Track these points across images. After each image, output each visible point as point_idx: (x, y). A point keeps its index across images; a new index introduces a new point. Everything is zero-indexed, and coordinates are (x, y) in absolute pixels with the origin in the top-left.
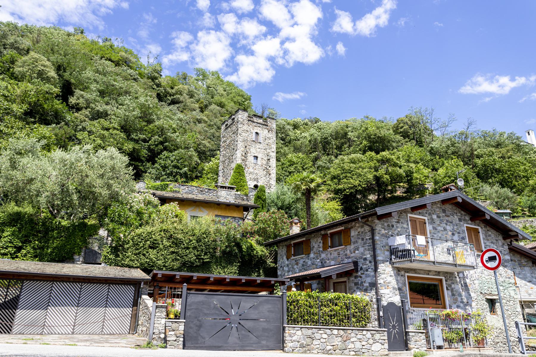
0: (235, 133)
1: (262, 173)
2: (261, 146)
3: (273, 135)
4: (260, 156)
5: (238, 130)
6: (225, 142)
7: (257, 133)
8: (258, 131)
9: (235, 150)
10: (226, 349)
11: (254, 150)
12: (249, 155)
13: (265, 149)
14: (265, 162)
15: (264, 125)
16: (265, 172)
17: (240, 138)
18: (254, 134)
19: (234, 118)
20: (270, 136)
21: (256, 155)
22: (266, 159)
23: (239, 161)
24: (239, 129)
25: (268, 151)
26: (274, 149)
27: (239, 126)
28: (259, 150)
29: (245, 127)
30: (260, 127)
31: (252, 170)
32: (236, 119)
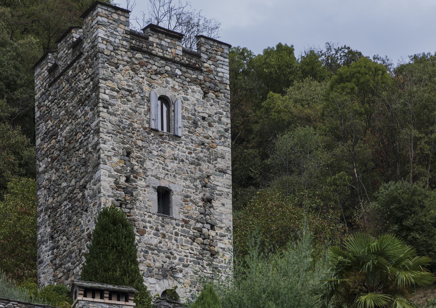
0: (90, 99)
1: (185, 250)
2: (181, 150)
3: (219, 110)
4: (178, 187)
5: (96, 88)
6: (51, 135)
7: (164, 99)
8: (169, 94)
9: (90, 164)
10: (161, 203)
11: (161, 167)
12: (141, 183)
13: (197, 163)
14: (194, 211)
15: (187, 66)
16: (196, 247)
17: (107, 121)
18: (155, 104)
19: (80, 41)
20: (212, 110)
21: (164, 184)
22: (198, 197)
23: (107, 201)
24: (102, 84)
25: (204, 166)
26: (226, 163)
27: (102, 72)
28: (172, 165)
29: (122, 78)
30: (173, 76)
31: (155, 241)
32: (86, 45)
